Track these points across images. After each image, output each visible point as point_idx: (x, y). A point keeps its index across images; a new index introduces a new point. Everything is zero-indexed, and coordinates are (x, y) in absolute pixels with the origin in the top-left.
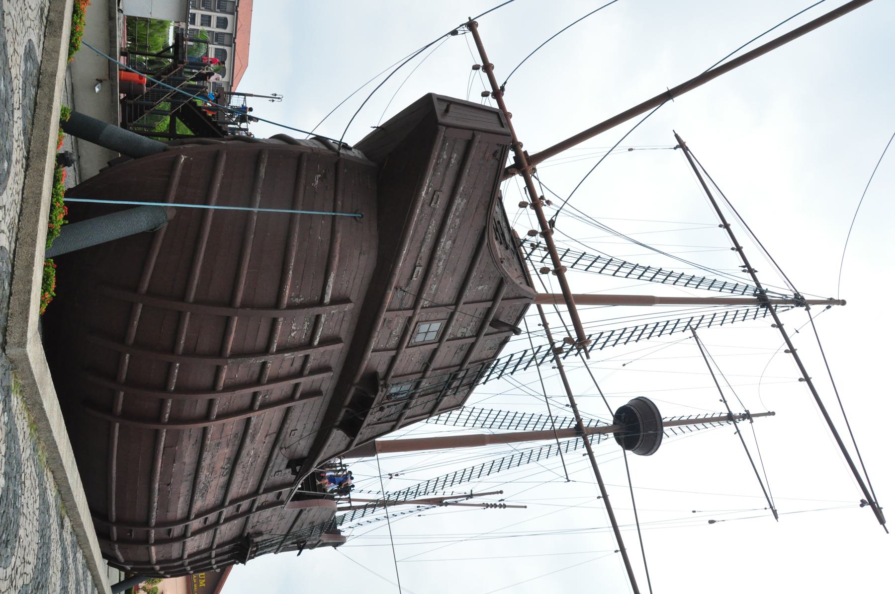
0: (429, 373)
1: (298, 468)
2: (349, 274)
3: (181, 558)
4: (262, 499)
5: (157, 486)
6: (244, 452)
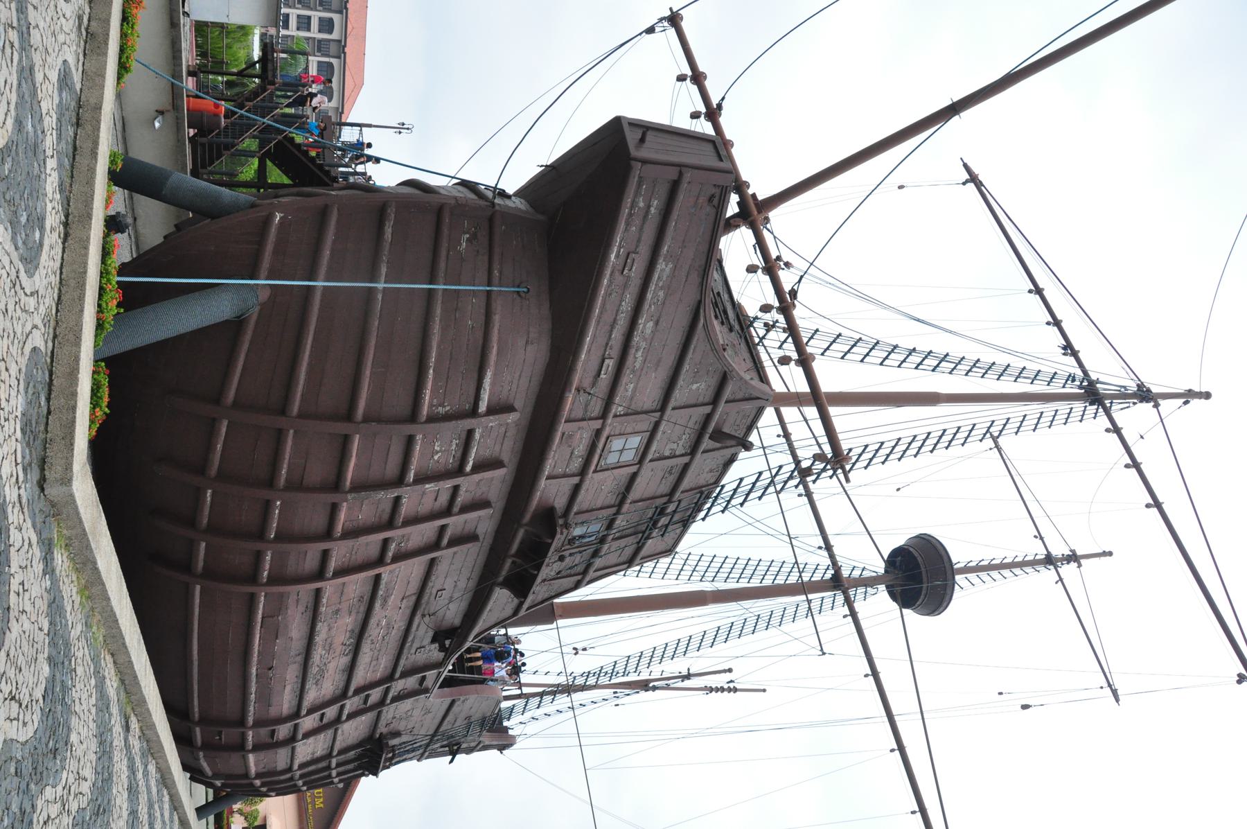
0: (626, 507)
1: (447, 642)
2: (513, 371)
3: (290, 769)
4: (399, 686)
5: (254, 671)
6: (373, 622)
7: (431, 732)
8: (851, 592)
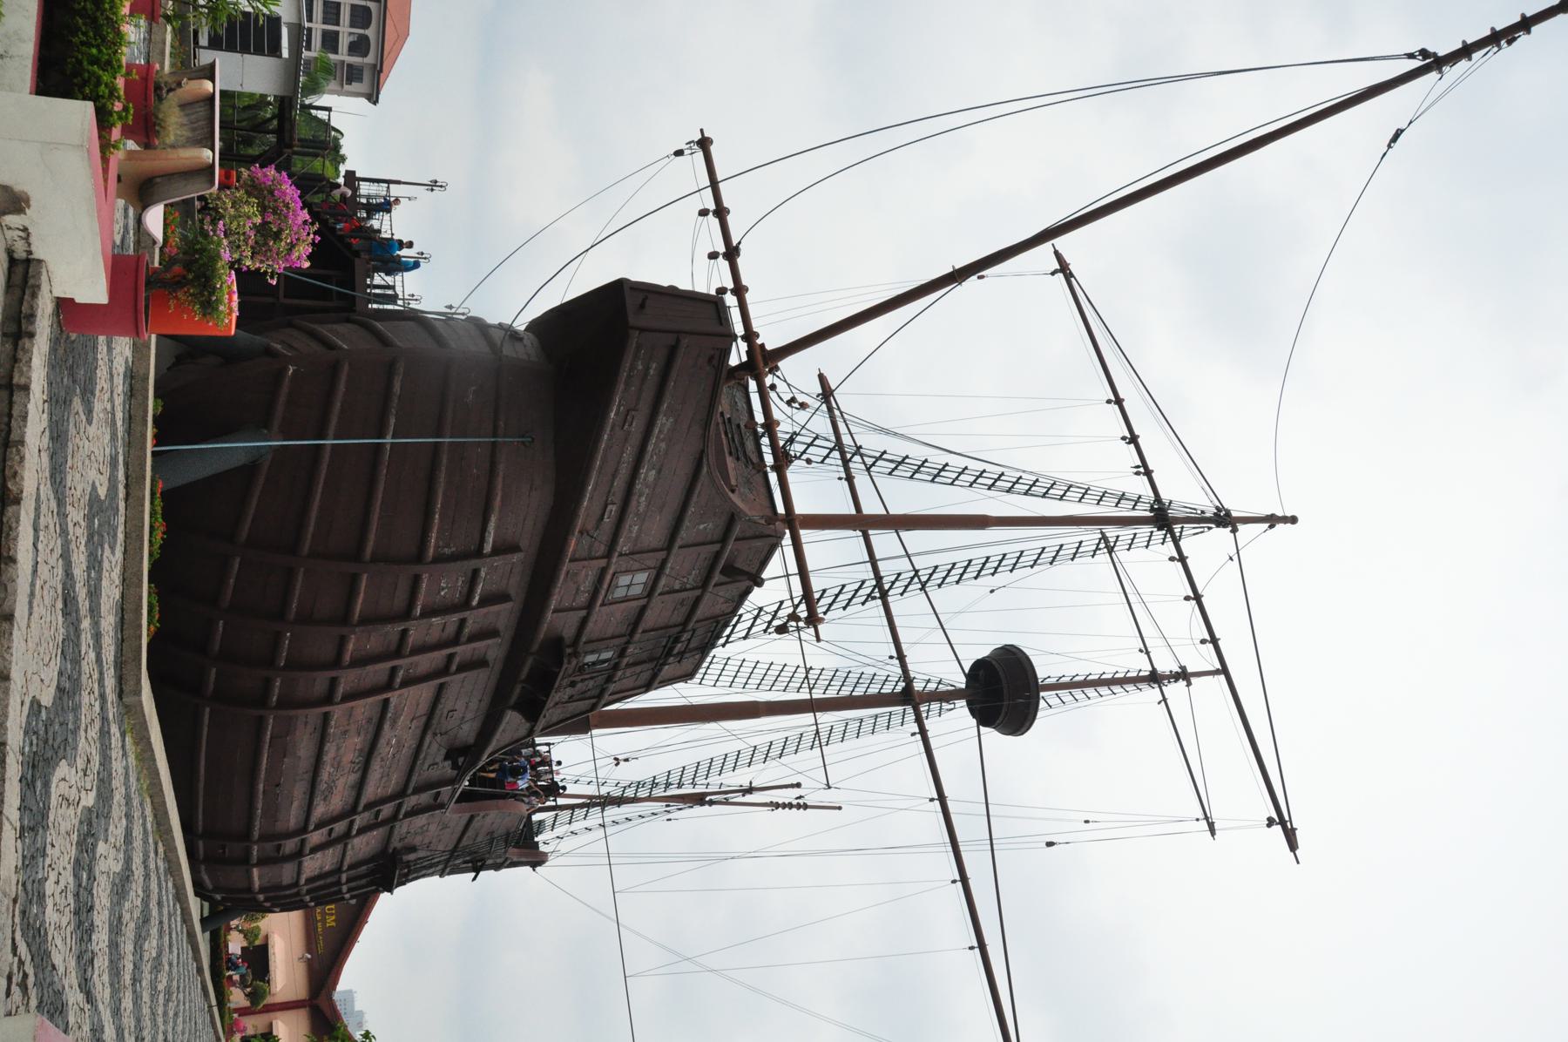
0: (637, 637)
1: (461, 760)
2: (517, 515)
3: (296, 884)
4: (412, 801)
5: (261, 787)
6: (382, 741)
7: (450, 847)
8: (923, 708)
